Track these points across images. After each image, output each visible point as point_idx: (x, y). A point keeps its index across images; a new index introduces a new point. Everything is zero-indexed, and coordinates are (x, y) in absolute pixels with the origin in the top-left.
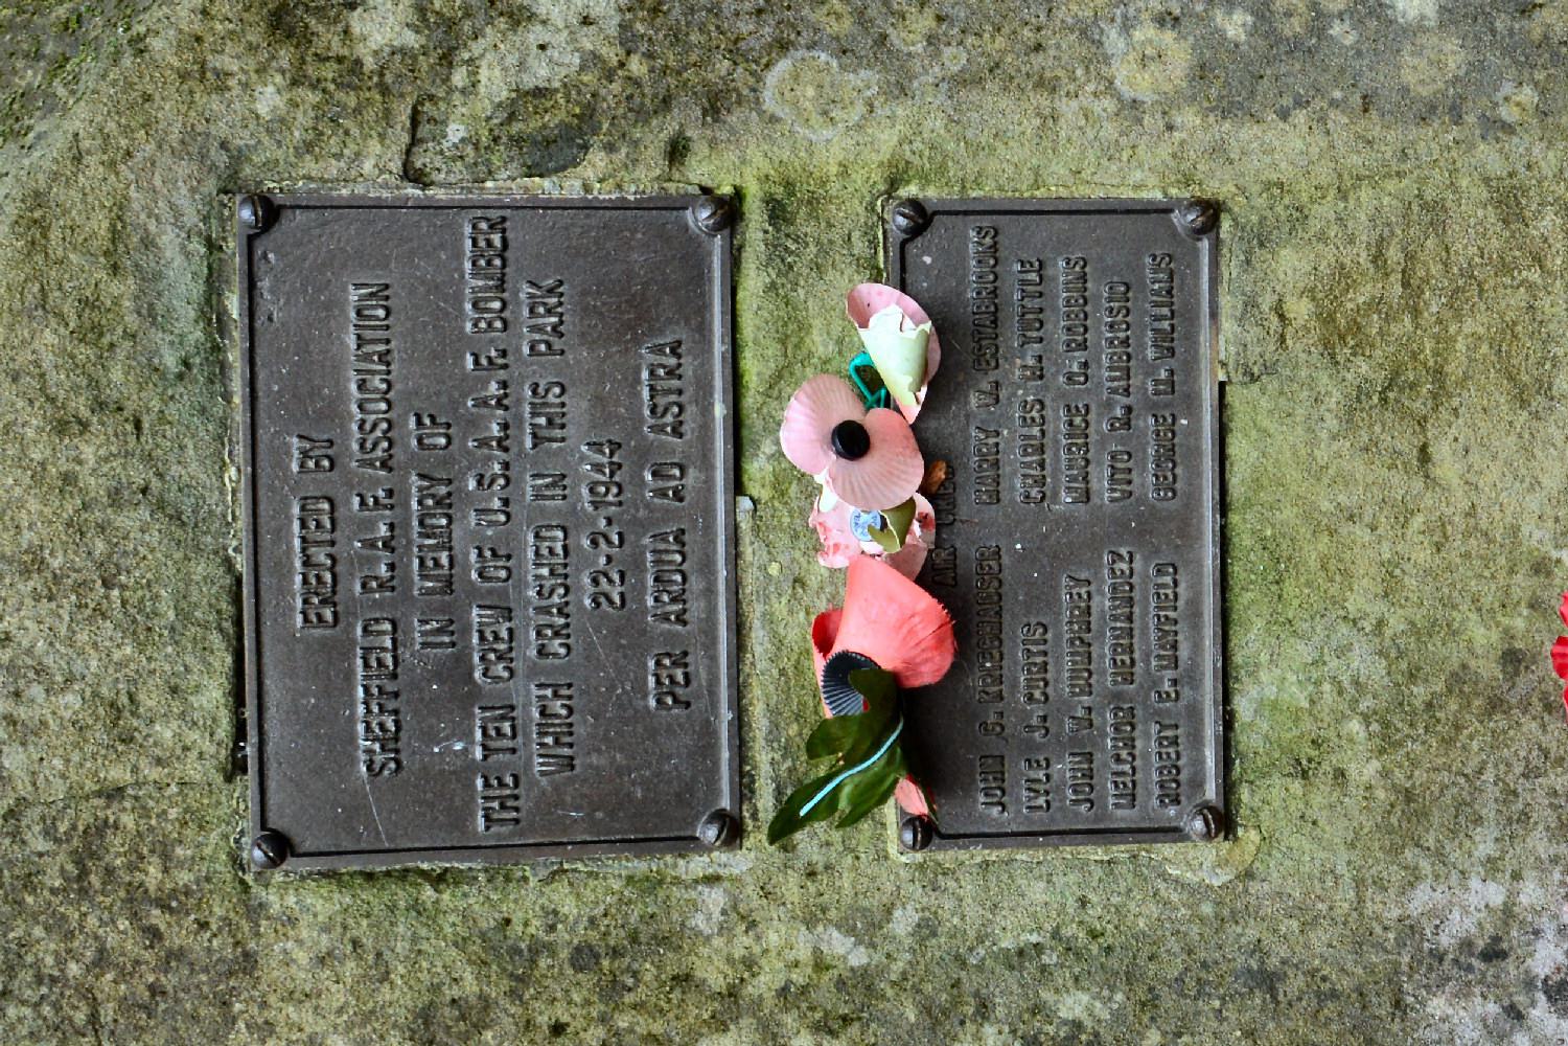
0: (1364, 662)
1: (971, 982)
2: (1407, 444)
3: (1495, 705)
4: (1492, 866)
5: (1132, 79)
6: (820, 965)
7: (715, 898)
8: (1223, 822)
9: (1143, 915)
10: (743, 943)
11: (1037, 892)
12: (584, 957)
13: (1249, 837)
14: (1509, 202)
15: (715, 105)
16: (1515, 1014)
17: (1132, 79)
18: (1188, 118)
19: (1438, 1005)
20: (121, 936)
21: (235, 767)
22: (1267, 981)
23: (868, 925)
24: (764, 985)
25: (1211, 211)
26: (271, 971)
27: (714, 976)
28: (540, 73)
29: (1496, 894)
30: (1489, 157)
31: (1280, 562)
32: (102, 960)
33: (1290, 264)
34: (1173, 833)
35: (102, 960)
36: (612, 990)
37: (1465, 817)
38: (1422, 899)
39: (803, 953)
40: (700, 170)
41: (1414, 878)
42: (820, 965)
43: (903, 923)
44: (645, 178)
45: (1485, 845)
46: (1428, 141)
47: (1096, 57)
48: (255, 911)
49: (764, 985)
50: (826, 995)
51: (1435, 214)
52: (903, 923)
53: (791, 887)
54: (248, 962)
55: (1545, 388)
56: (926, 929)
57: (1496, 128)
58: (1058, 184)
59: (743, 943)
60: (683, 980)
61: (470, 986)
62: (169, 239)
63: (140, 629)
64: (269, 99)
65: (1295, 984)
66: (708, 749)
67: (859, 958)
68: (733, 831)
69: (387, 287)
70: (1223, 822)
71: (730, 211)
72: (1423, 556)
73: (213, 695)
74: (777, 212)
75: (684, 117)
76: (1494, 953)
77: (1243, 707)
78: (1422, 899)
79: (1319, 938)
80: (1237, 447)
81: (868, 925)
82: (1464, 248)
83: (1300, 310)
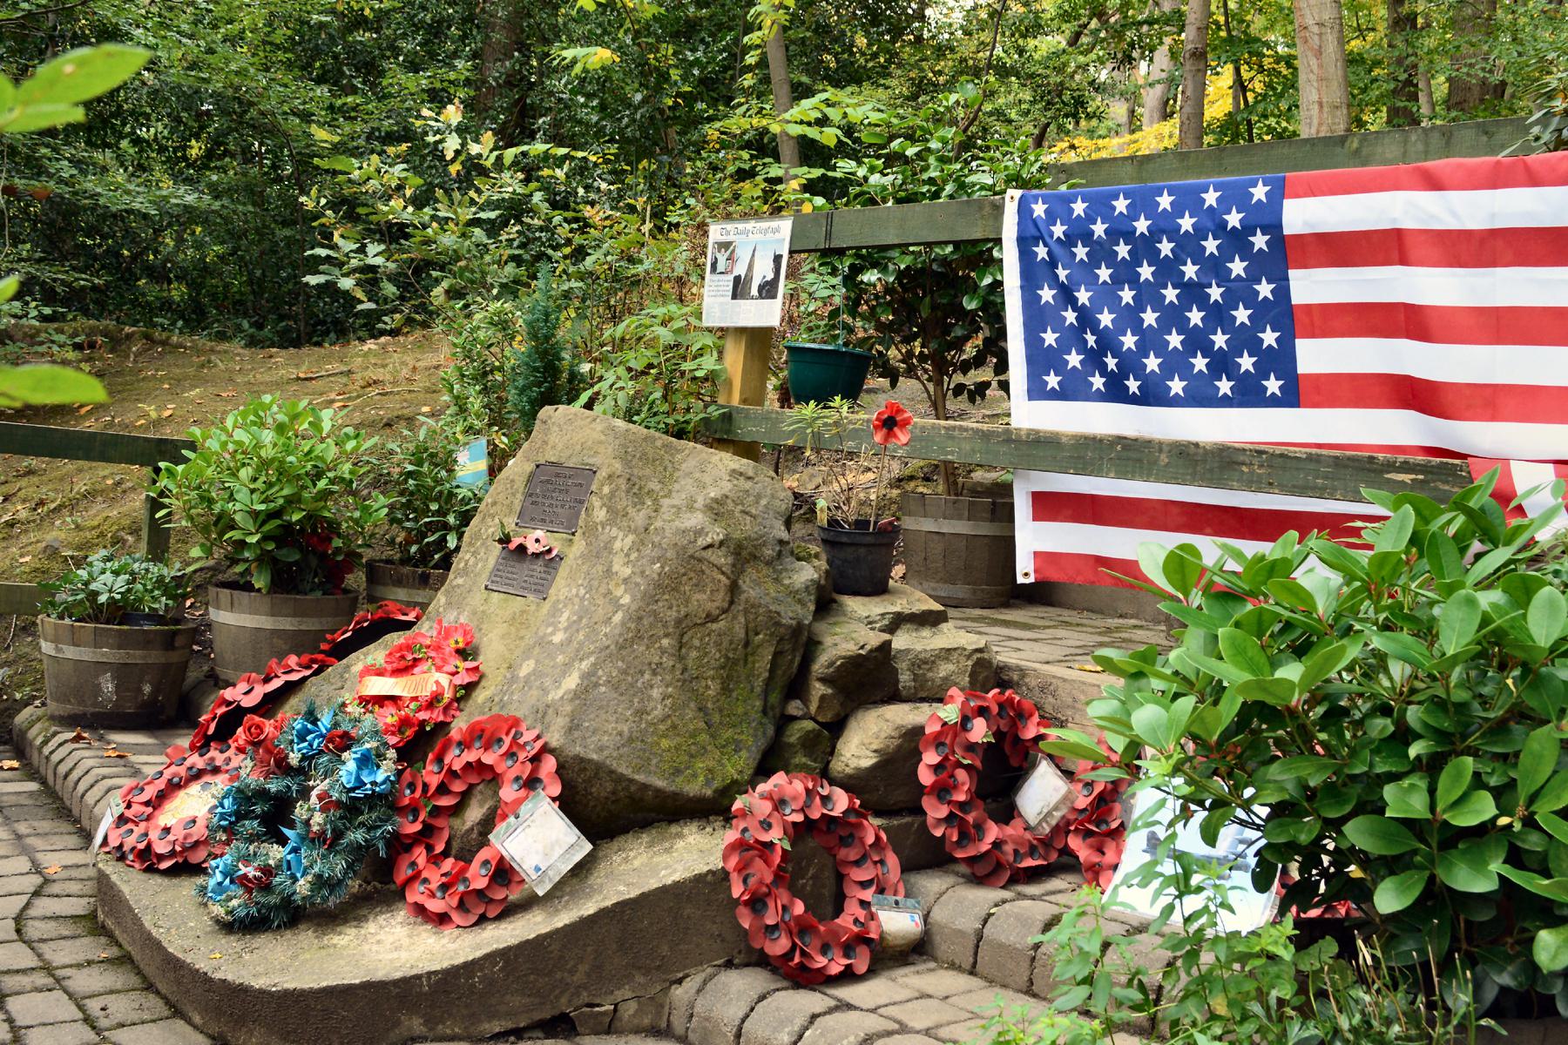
31: (506, 600)
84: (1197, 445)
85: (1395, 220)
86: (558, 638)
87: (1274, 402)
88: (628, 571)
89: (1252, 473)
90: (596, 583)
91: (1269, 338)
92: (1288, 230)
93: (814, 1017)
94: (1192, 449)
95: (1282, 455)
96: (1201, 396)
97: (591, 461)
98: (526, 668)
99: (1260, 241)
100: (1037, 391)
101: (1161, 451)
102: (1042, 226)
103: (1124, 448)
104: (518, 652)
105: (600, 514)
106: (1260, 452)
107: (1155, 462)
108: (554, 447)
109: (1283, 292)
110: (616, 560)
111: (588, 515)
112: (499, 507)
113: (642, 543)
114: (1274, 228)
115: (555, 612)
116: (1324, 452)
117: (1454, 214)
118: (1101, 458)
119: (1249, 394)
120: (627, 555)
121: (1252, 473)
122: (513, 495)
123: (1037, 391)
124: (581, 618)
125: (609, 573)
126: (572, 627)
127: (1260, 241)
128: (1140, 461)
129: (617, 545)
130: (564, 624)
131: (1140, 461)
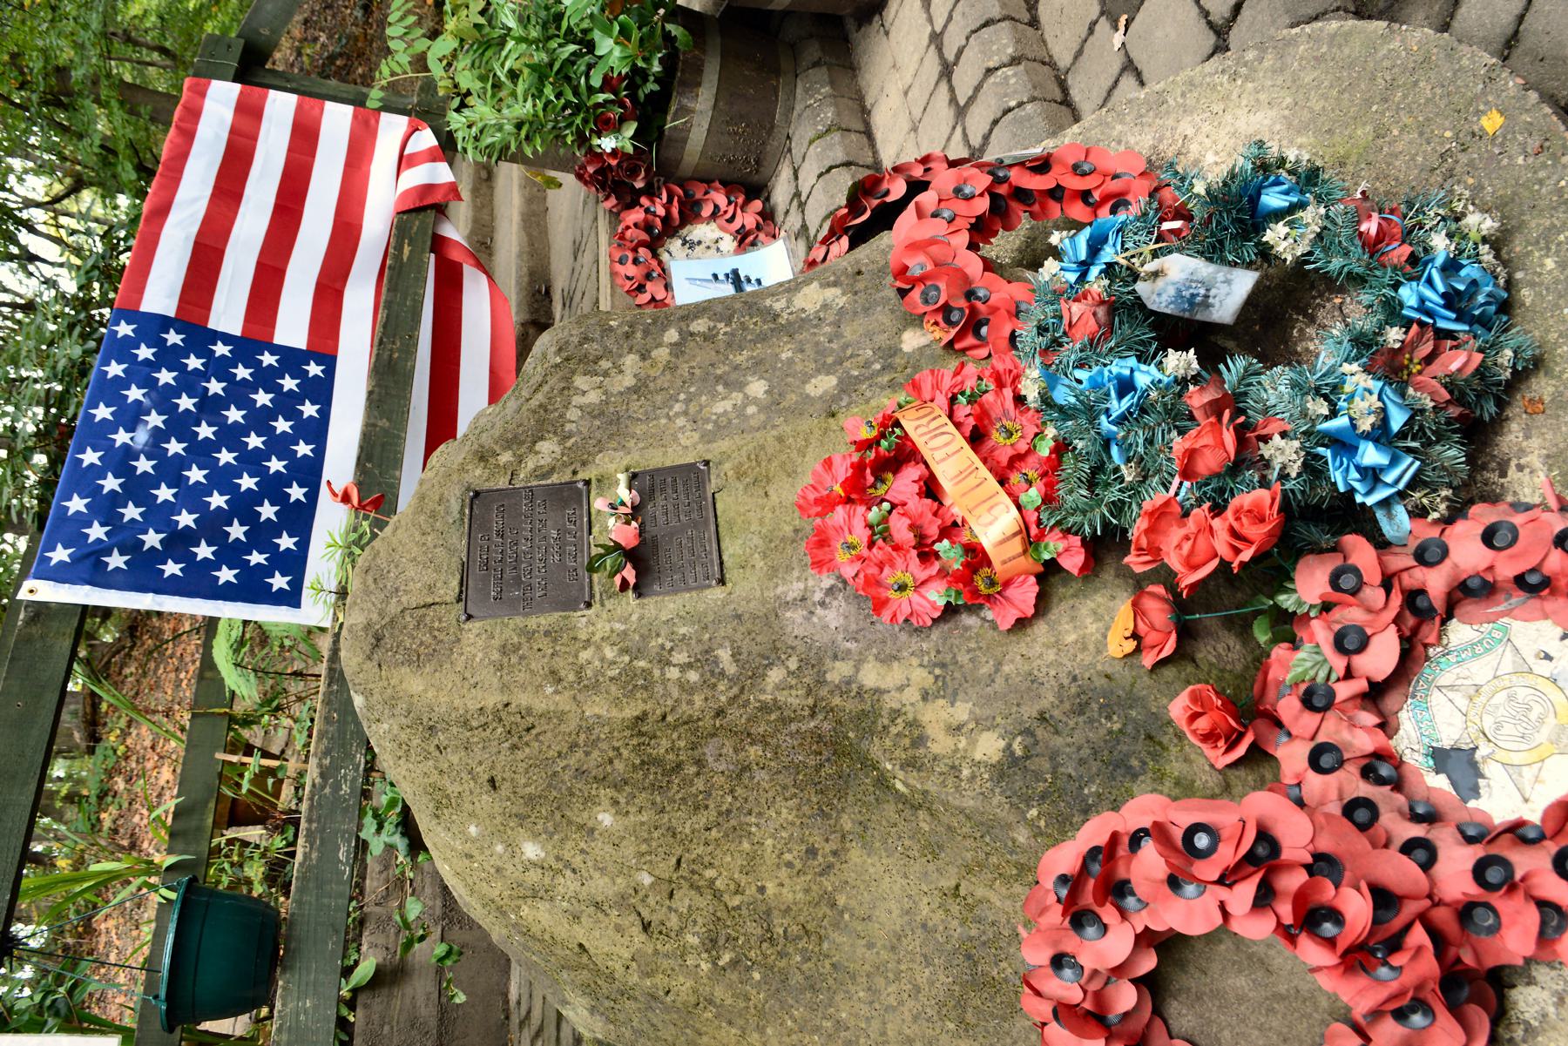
0: (756, 540)
1: (654, 629)
2: (761, 492)
3: (793, 541)
4: (799, 579)
5: (684, 442)
6: (612, 631)
7: (584, 620)
8: (722, 581)
9: (701, 607)
10: (591, 629)
11: (672, 606)
12: (547, 633)
13: (729, 585)
14: (780, 439)
15: (584, 464)
16: (812, 613)
17: (684, 442)
18: (700, 446)
19: (788, 614)
20: (427, 638)
21: (459, 600)
22: (739, 617)
23: (625, 620)
24: (597, 638)
25: (707, 463)
26: (464, 642)
27: (583, 636)
28: (542, 462)
29: (801, 585)
30: (774, 433)
31: (731, 524)
32: (422, 643)
33: (727, 466)
34: (710, 586)
35: (422, 643)
36: (555, 640)
37: (789, 569)
38: (779, 590)
39: (608, 628)
40: (580, 476)
41: (777, 586)
42: (612, 631)
43: (634, 618)
44: (567, 477)
45: (796, 573)
46: (758, 435)
47: (676, 439)
48: (461, 630)
49: (597, 638)
50: (614, 638)
51: (762, 447)
52: (634, 618)
53: (604, 616)
54: (459, 640)
55: (795, 472)
56: (641, 618)
57: (774, 427)
58: (668, 464)
59: (591, 629)
60: (575, 639)
61: (516, 639)
62: (453, 501)
63: (438, 570)
64: (478, 472)
65: (746, 616)
66: (582, 589)
67: (623, 627)
68: (589, 605)
69: (514, 747)
70: (722, 581)
71: (588, 483)
72: (770, 515)
73: (455, 583)
74: (599, 481)
75: (577, 466)
76: (803, 599)
77: (725, 558)
78: (779, 590)
79: (752, 605)
80: (718, 506)
81: (625, 620)
82: (770, 451)
83: (730, 473)
84: (370, 393)
85: (187, 238)
86: (757, 388)
87: (330, 372)
88: (630, 361)
89: (399, 350)
90: (659, 399)
91: (268, 359)
92: (171, 312)
93: (990, 71)
94: (375, 396)
95: (385, 326)
96: (317, 431)
97: (455, 506)
98: (823, 384)
99: (173, 338)
100: (291, 598)
101: (374, 425)
102: (86, 550)
103: (369, 459)
104: (805, 424)
105: (548, 449)
106: (381, 342)
107: (386, 432)
108: (431, 588)
109: (227, 339)
110: (616, 388)
111: (552, 470)
112: (559, 663)
113: (584, 359)
114: (164, 323)
115: (722, 427)
116: (383, 298)
117: (195, 200)
118: (379, 484)
119: (322, 391)
120: (606, 374)
121: (399, 350)
122: (529, 635)
123: (291, 598)
124: (718, 379)
125: (640, 388)
126: (734, 384)
127: (173, 338)
128: (383, 445)
129: (593, 397)
130: (737, 397)
131: (383, 445)
